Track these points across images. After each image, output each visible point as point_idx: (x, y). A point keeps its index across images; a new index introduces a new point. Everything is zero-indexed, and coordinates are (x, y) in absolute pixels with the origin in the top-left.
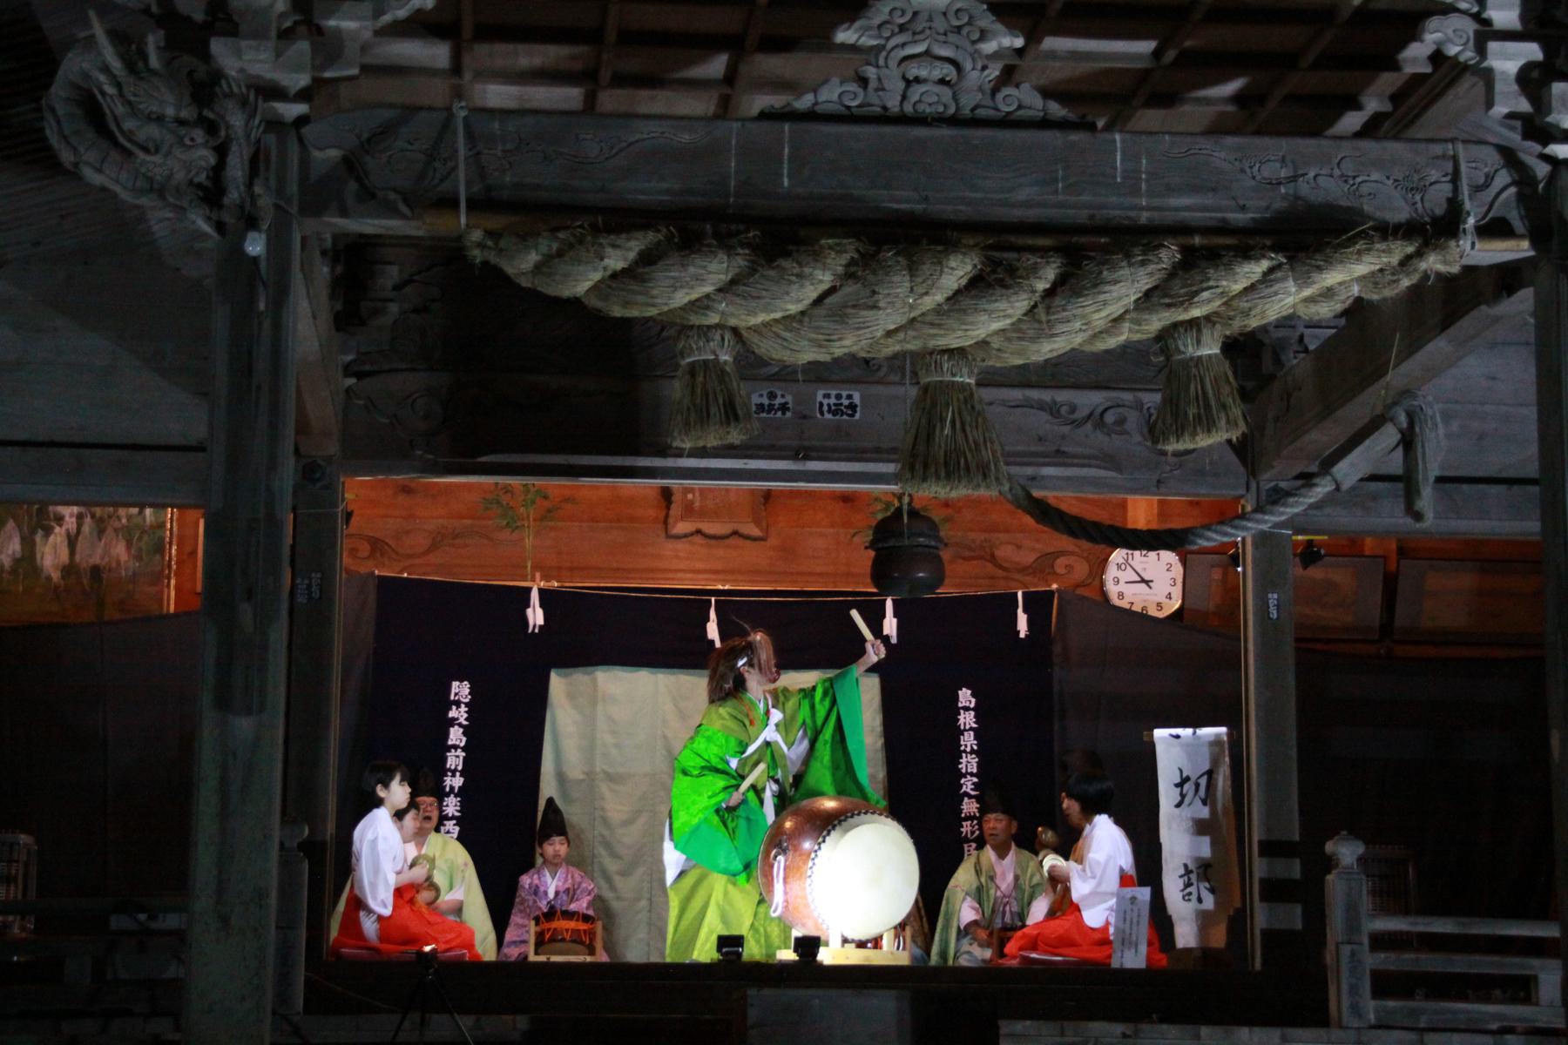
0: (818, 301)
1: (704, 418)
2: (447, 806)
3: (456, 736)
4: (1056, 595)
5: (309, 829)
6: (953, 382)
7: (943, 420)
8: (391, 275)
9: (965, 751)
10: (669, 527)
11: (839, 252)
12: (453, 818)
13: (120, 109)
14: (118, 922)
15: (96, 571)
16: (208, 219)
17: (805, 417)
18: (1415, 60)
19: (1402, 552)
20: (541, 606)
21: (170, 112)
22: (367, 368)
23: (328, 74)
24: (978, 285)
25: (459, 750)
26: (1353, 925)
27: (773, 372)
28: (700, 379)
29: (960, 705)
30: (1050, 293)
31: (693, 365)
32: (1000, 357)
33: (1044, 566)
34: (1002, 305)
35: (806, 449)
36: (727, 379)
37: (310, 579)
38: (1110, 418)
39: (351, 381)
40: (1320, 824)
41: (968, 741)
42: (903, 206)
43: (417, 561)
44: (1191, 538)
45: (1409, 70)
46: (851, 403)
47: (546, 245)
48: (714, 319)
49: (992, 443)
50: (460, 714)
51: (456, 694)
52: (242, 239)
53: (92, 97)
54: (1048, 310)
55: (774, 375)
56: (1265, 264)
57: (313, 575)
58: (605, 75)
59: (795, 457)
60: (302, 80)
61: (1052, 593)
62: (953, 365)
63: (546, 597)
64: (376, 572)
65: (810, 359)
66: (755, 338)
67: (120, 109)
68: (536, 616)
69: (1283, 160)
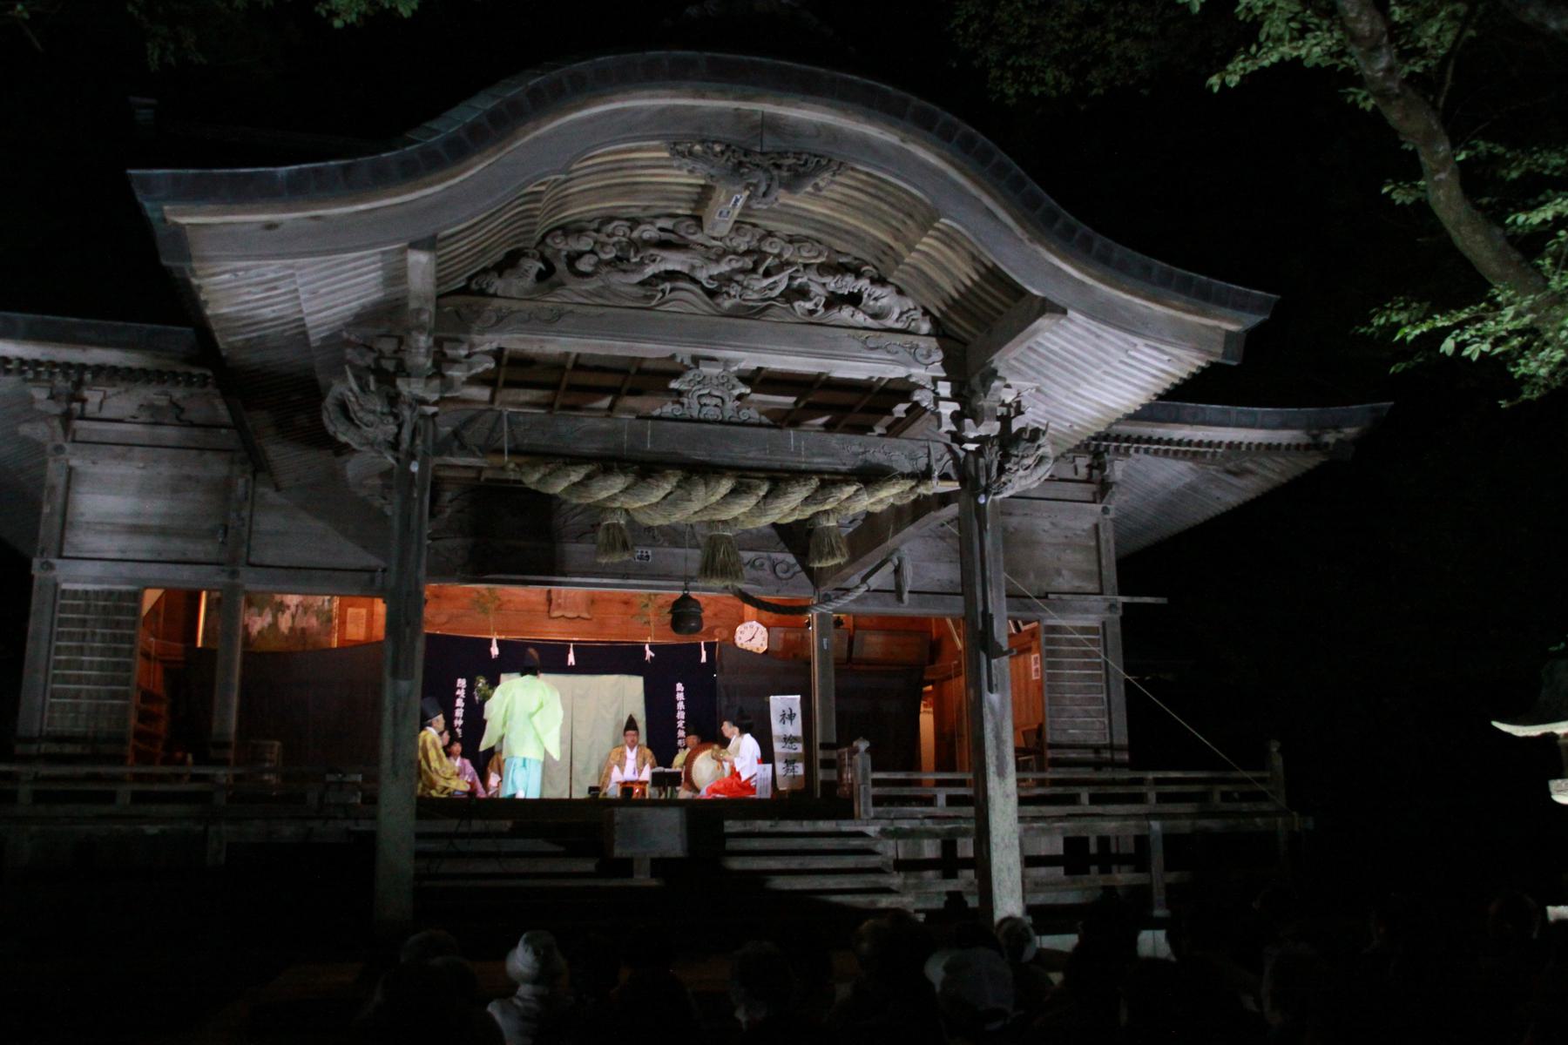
0: (665, 498)
7: (719, 551)
8: (448, 496)
11: (675, 476)
13: (357, 408)
14: (330, 778)
15: (303, 630)
16: (393, 456)
18: (899, 412)
19: (855, 627)
21: (379, 408)
22: (436, 536)
23: (447, 395)
24: (734, 492)
26: (865, 776)
28: (611, 531)
30: (765, 497)
34: (744, 501)
35: (628, 574)
38: (757, 563)
39: (429, 542)
40: (846, 737)
41: (681, 705)
42: (701, 458)
45: (897, 415)
47: (543, 470)
48: (617, 504)
52: (409, 464)
53: (345, 402)
54: (764, 504)
56: (854, 488)
58: (557, 405)
60: (435, 397)
61: (715, 643)
63: (500, 643)
66: (636, 514)
67: (357, 408)
68: (495, 651)
69: (860, 445)
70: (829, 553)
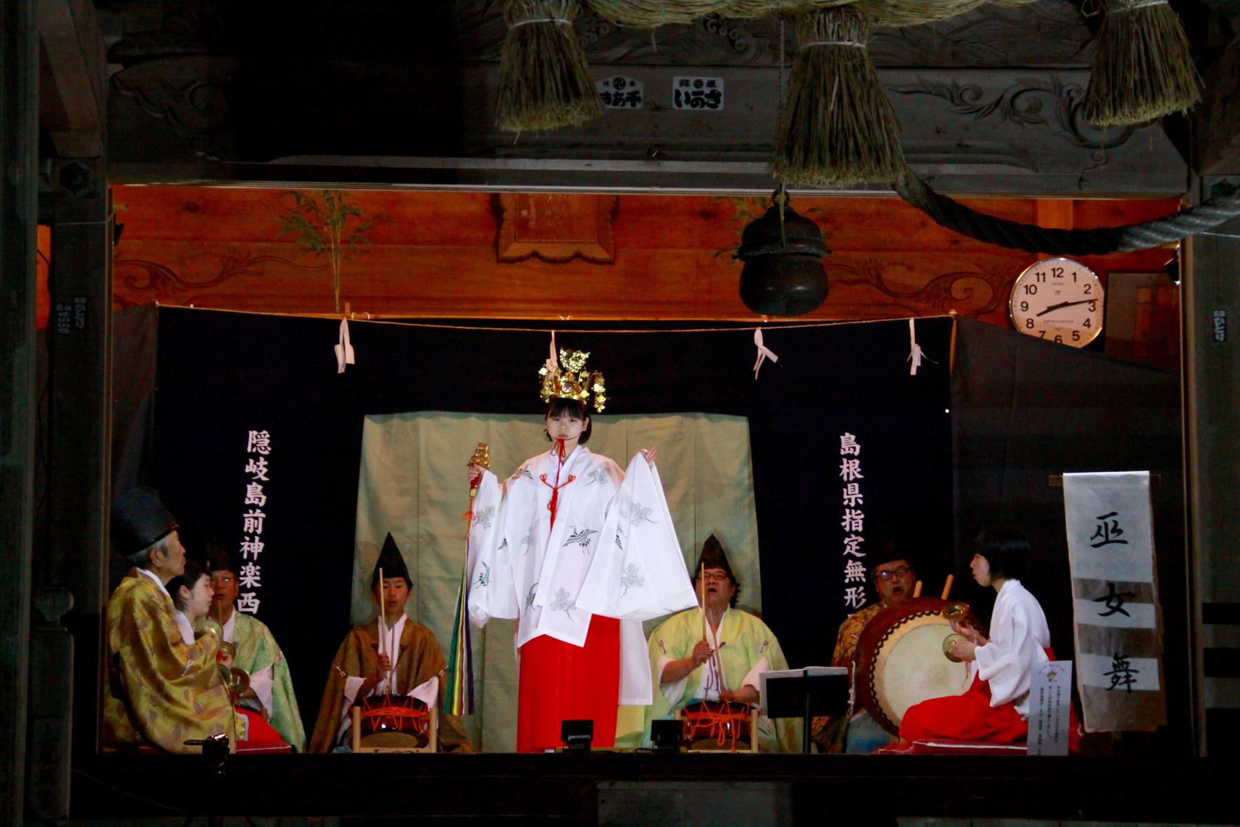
1: (537, 94)
2: (245, 575)
3: (254, 494)
4: (955, 323)
5: (75, 599)
6: (839, 47)
7: (827, 94)
9: (848, 506)
10: (500, 249)
12: (253, 589)
17: (658, 109)
20: (352, 343)
22: (137, 52)
25: (258, 511)
27: (620, 55)
28: (532, 47)
29: (842, 453)
31: (523, 31)
32: (893, 15)
33: (939, 292)
35: (661, 146)
36: (565, 48)
37: (73, 305)
38: (1022, 103)
39: (117, 68)
41: (852, 494)
43: (207, 291)
44: (1127, 238)
46: (713, 92)
49: (886, 120)
50: (258, 468)
51: (253, 446)
55: (620, 59)
57: (77, 300)
59: (647, 157)
62: (840, 26)
64: (157, 303)
65: (665, 22)
68: (345, 354)
70: (1140, 87)
